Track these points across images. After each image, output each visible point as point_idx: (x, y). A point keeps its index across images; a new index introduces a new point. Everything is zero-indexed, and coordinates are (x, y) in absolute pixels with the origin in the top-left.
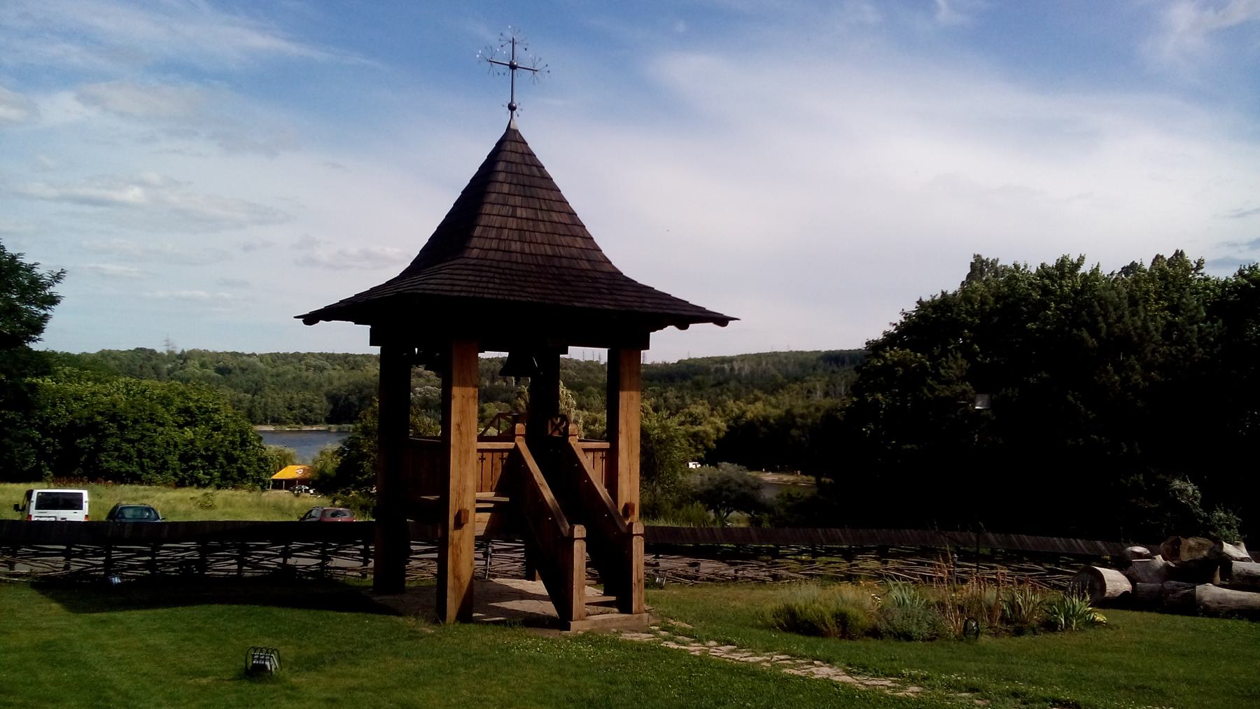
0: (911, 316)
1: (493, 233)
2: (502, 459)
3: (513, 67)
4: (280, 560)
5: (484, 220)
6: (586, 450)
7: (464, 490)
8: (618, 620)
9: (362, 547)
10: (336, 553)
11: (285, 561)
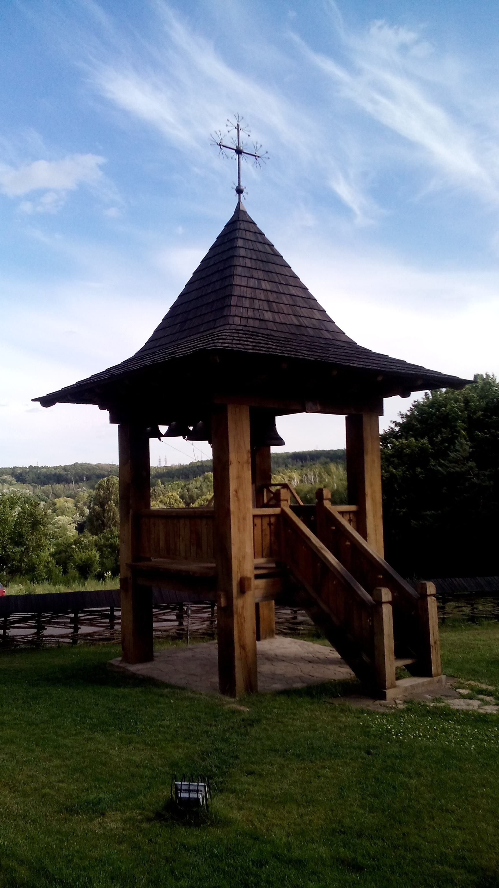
0: (407, 416)
1: (247, 303)
2: (270, 524)
3: (239, 152)
6: (342, 513)
7: (244, 557)
8: (423, 684)
9: (72, 615)
10: (49, 623)
11: (5, 632)
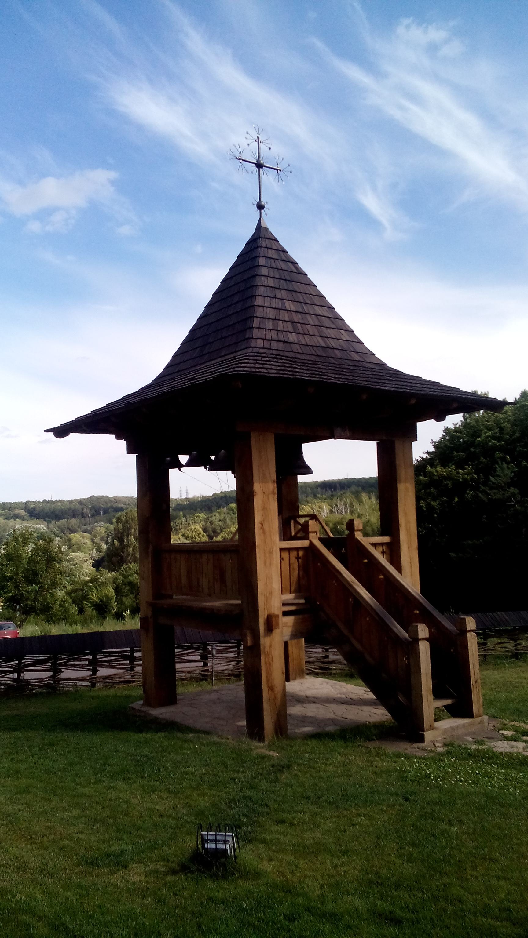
1: (270, 325)
2: (298, 558)
3: (259, 166)
4: (15, 675)
5: (259, 312)
6: (375, 545)
7: (271, 593)
8: (464, 726)
9: (90, 657)
10: (65, 665)
11: (19, 676)
